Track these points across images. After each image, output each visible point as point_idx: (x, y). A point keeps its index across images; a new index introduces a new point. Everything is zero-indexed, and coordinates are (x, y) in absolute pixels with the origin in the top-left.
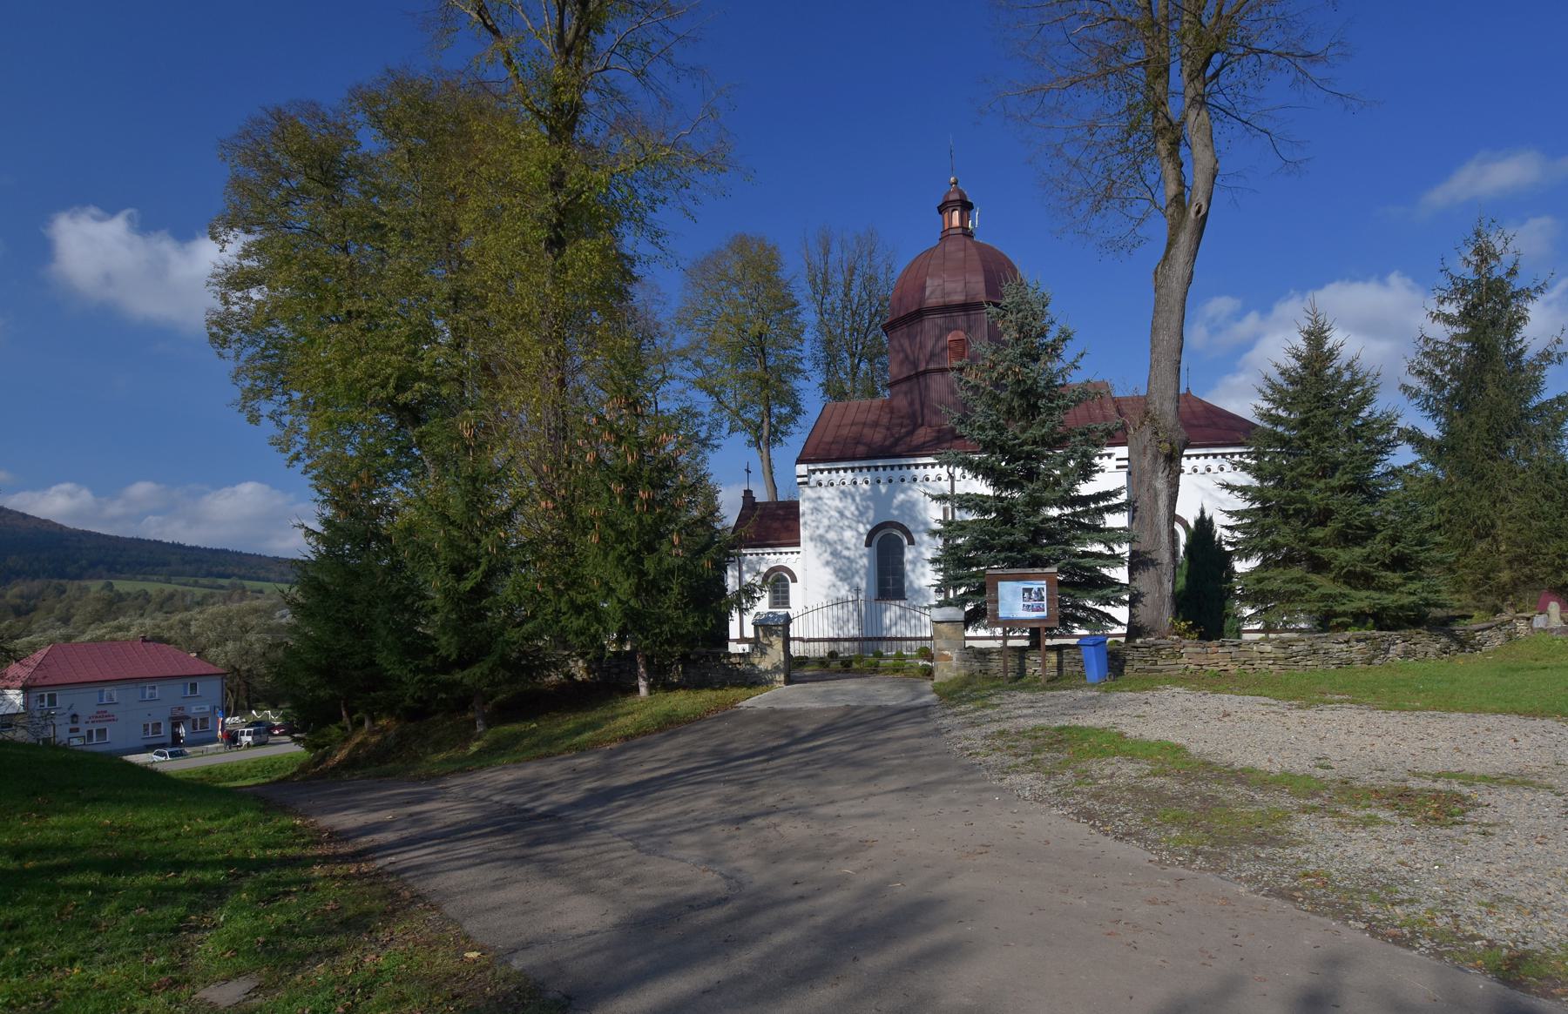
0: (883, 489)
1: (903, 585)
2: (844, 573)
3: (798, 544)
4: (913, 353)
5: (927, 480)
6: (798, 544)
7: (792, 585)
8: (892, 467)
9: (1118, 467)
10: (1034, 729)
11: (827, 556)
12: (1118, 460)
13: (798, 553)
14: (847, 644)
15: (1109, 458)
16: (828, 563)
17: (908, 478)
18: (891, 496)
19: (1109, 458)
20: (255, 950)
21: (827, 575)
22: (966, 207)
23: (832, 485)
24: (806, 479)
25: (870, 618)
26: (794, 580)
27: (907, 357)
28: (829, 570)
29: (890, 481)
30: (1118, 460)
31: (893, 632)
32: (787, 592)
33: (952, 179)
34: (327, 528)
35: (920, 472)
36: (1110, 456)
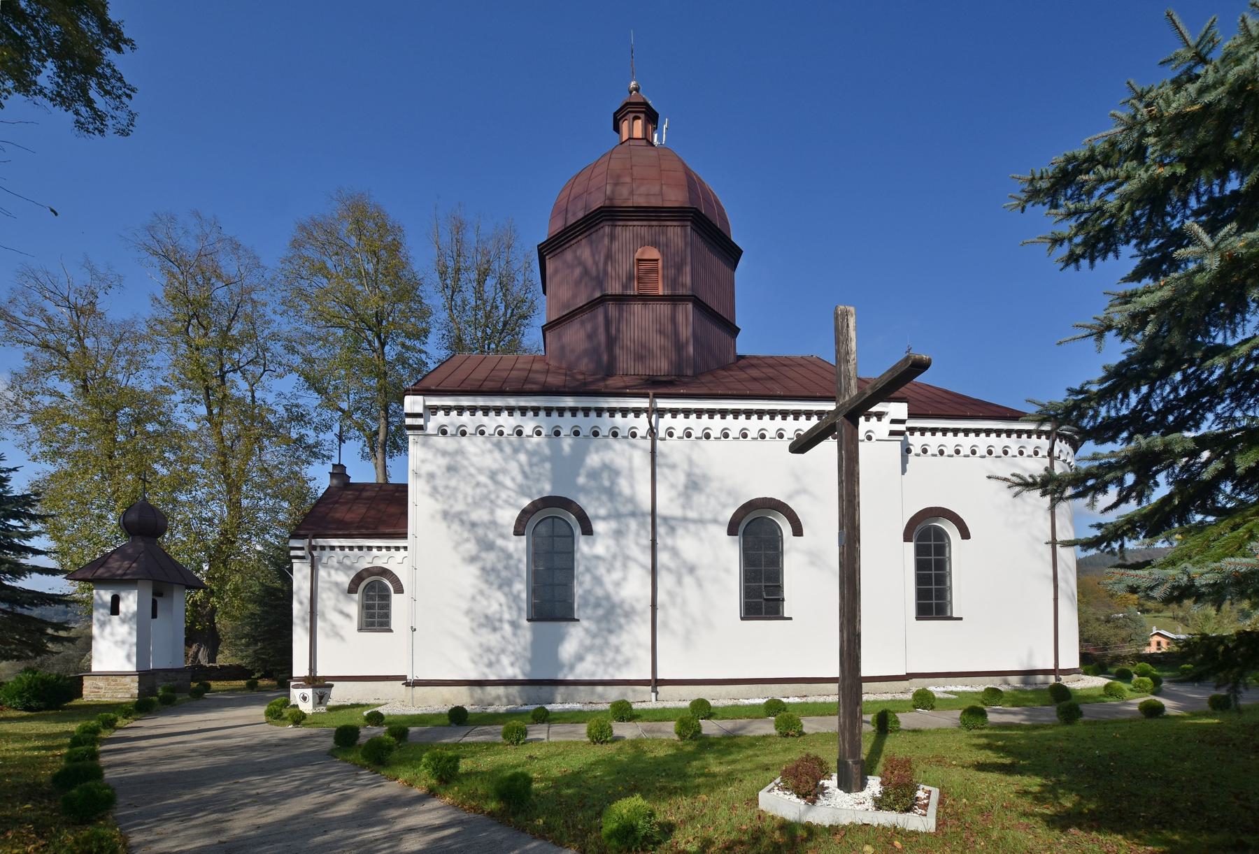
0: (567, 443)
1: (571, 595)
2: (495, 577)
3: (404, 536)
4: (596, 264)
5: (634, 435)
6: (404, 536)
7: (395, 598)
8: (586, 411)
9: (892, 433)
10: (1178, 639)
11: (471, 547)
12: (893, 421)
13: (405, 548)
14: (501, 690)
15: (879, 419)
16: (473, 559)
17: (604, 431)
18: (579, 456)
19: (879, 419)
20: (1173, 759)
21: (469, 577)
22: (652, 118)
23: (482, 433)
24: (420, 421)
25: (544, 650)
26: (399, 589)
27: (586, 272)
28: (474, 570)
29: (577, 433)
30: (893, 421)
31: (583, 671)
32: (388, 606)
33: (633, 84)
34: (1197, 445)
35: (606, 422)
36: (880, 416)
